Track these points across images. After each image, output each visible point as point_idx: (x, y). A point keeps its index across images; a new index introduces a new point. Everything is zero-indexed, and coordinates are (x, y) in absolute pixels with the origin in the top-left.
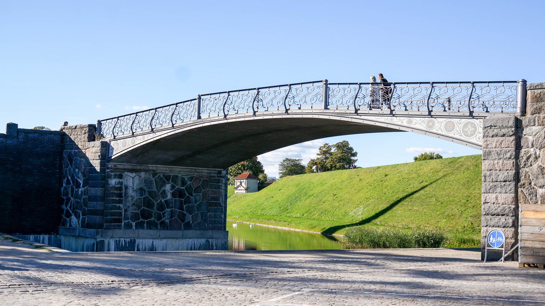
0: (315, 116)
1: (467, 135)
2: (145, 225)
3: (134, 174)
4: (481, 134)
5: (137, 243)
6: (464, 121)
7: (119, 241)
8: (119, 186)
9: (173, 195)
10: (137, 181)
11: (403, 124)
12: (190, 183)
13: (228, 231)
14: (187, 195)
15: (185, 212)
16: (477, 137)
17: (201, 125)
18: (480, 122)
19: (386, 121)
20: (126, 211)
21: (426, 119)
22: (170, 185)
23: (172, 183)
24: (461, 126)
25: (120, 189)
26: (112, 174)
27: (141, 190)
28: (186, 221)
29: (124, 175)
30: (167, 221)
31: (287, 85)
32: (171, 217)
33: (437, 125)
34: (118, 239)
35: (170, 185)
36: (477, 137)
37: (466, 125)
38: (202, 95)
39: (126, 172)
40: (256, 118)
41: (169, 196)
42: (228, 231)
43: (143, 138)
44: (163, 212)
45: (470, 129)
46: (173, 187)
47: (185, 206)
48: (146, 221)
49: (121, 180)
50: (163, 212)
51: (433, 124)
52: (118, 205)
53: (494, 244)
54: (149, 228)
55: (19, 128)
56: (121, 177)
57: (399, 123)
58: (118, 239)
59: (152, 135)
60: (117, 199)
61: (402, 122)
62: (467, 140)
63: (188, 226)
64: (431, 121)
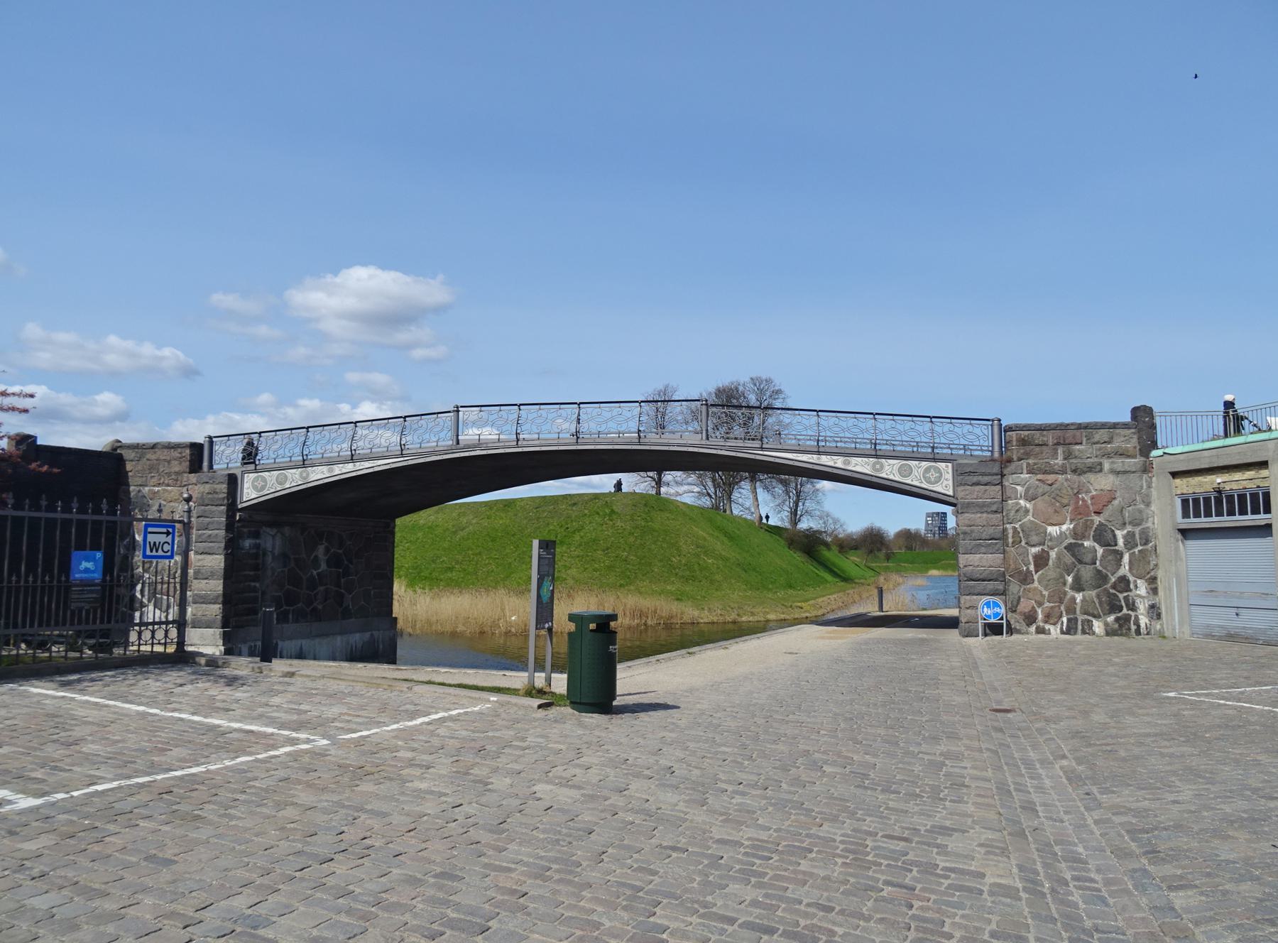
0: (691, 449)
1: (930, 482)
2: (291, 616)
3: (273, 531)
4: (268, 479)
5: (279, 647)
6: (925, 464)
7: (255, 646)
8: (254, 551)
9: (328, 563)
10: (278, 542)
11: (837, 465)
12: (349, 543)
13: (396, 619)
14: (346, 562)
15: (342, 591)
16: (944, 485)
17: (467, 454)
18: (947, 467)
19: (811, 461)
20: (263, 593)
21: (871, 459)
22: (323, 546)
23: (326, 544)
24: (921, 471)
25: (256, 556)
26: (245, 530)
27: (284, 556)
28: (344, 606)
29: (262, 532)
30: (320, 607)
31: (516, 405)
32: (326, 600)
33: (887, 468)
34: (253, 644)
35: (323, 546)
36: (944, 485)
37: (927, 470)
38: (462, 407)
39: (264, 528)
40: (520, 450)
41: (323, 566)
42: (396, 619)
43: (332, 471)
44: (315, 592)
45: (933, 475)
46: (327, 550)
47: (342, 580)
48: (292, 608)
49: (258, 541)
50: (315, 592)
51: (882, 467)
52: (253, 584)
53: (990, 617)
54: (296, 621)
55: (39, 442)
56: (256, 535)
57: (831, 464)
58: (253, 644)
59: (350, 467)
60: (252, 573)
61: (835, 463)
62: (930, 488)
63: (346, 614)
64: (878, 463)
